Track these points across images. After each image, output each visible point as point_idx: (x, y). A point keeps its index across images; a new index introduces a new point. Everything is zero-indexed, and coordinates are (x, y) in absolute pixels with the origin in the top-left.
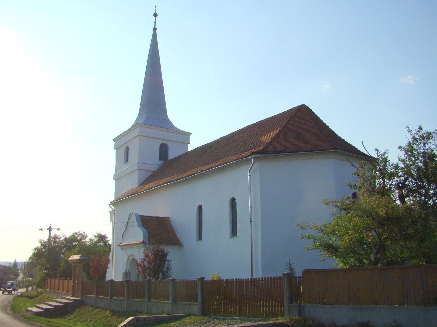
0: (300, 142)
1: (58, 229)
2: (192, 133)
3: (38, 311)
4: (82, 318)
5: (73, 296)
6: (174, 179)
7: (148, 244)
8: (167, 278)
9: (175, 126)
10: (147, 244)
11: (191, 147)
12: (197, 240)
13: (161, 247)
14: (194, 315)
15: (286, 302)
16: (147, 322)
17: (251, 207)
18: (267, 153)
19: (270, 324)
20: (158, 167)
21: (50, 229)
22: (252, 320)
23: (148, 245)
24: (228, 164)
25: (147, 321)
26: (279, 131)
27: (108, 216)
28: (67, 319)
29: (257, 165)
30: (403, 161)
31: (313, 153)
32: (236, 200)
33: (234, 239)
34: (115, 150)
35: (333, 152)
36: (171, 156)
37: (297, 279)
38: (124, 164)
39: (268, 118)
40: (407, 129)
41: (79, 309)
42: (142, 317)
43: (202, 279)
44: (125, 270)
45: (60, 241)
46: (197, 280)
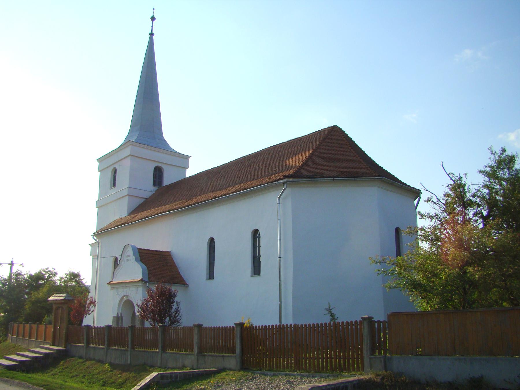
0: (341, 167)
1: (22, 265)
2: (191, 157)
3: (10, 364)
4: (71, 373)
5: (54, 345)
6: (176, 207)
7: (148, 283)
8: (175, 323)
9: (172, 147)
10: (147, 283)
11: (190, 172)
12: (207, 280)
13: (167, 286)
14: (230, 370)
15: (366, 354)
16: (174, 379)
17: (280, 240)
18: (301, 177)
19: (356, 380)
20: (151, 194)
21: (12, 264)
22: (316, 376)
23: (148, 284)
24: (251, 189)
25: (174, 377)
26: (311, 154)
27: (88, 249)
28: (50, 374)
29: (288, 191)
30: (485, 186)
31: (355, 179)
32: (215, 240)
33: (257, 279)
34: (99, 172)
35: (377, 179)
36: (167, 181)
37: (381, 324)
38: (110, 189)
39: (291, 140)
40: (489, 151)
41: (63, 361)
42: (168, 373)
43: (199, 326)
44: (117, 313)
45: (24, 279)
46: (234, 326)
